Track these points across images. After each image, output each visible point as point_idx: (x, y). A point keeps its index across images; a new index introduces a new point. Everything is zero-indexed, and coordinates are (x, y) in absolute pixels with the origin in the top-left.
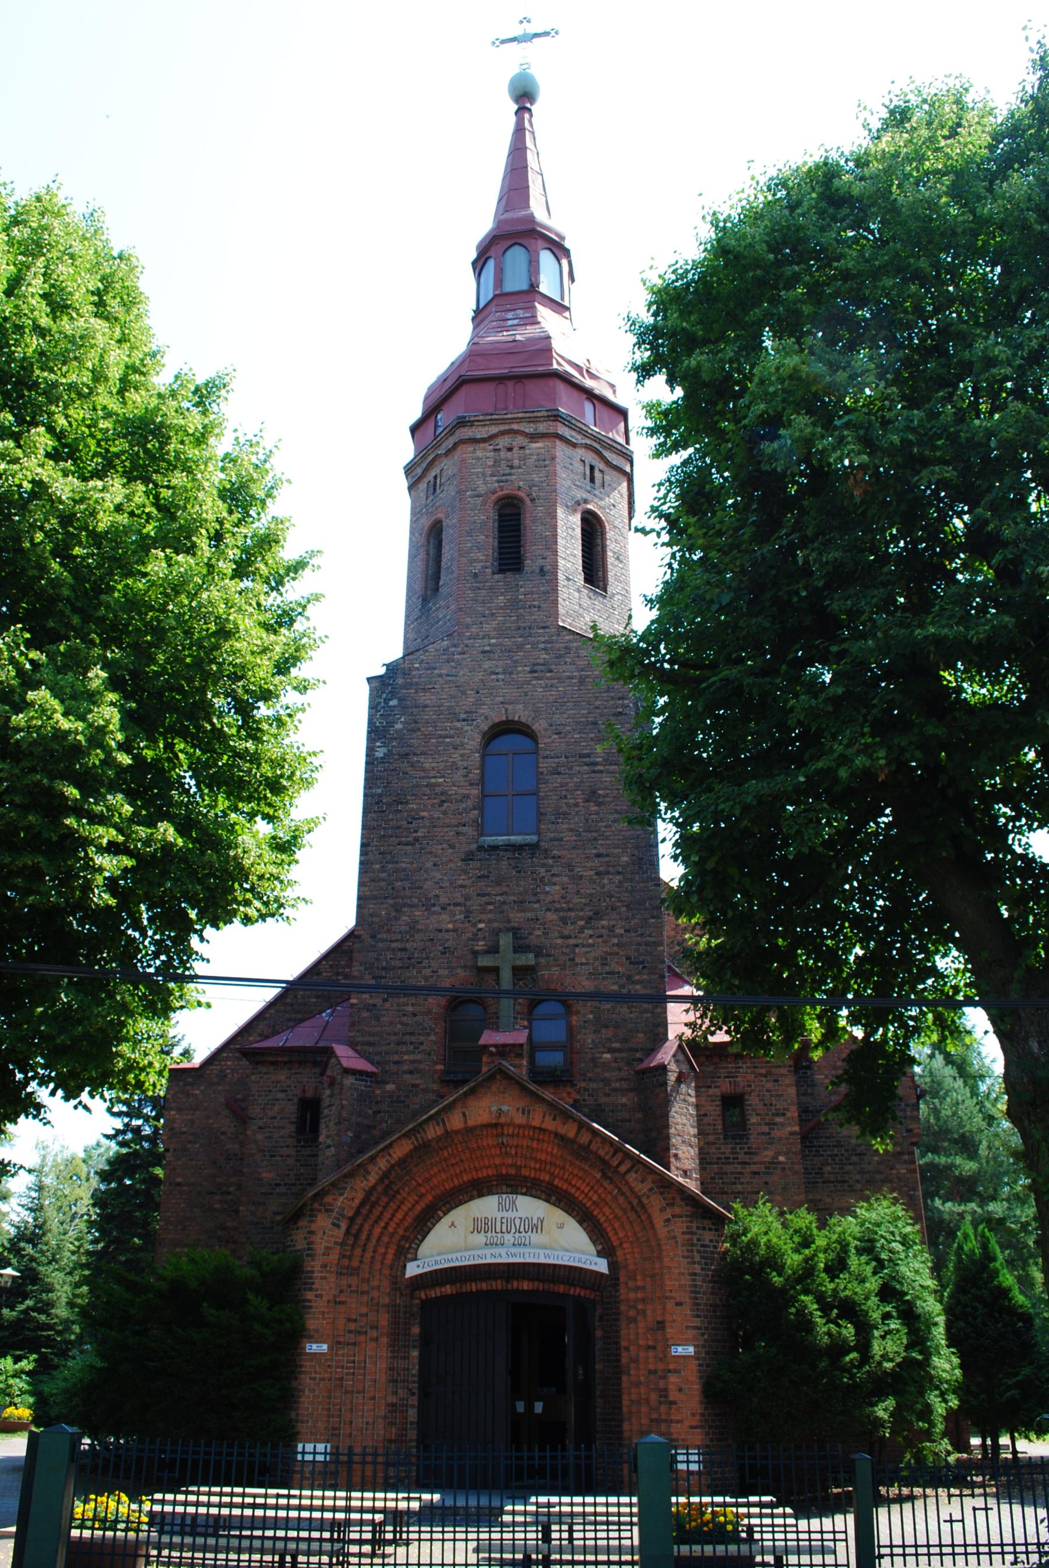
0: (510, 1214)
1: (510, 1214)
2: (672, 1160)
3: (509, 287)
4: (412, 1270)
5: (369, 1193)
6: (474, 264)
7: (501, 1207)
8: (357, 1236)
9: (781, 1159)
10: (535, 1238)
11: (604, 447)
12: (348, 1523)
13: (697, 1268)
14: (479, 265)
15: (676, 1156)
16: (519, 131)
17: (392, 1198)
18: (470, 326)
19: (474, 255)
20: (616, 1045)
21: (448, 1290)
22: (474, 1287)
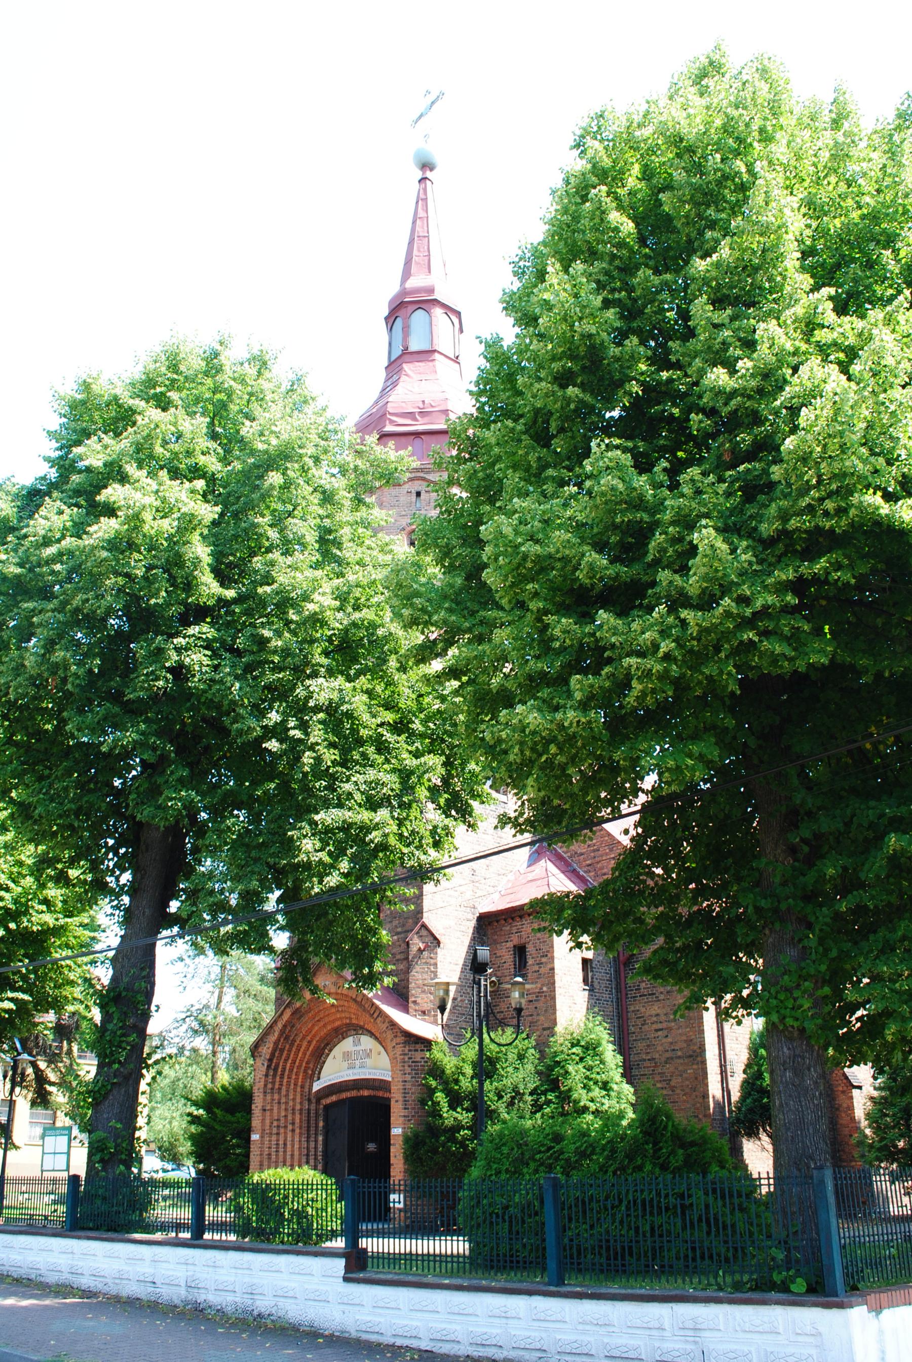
0: (358, 1048)
1: (358, 1048)
2: (411, 1005)
3: (413, 347)
4: (317, 1087)
5: (276, 1043)
6: (386, 319)
7: (355, 1044)
8: (276, 1070)
9: (545, 989)
10: (368, 1061)
11: (428, 473)
12: (442, 1192)
13: (408, 1077)
14: (391, 318)
15: (415, 1002)
16: (422, 200)
17: (292, 1045)
18: (383, 374)
19: (386, 313)
20: (399, 930)
21: (334, 1098)
22: (344, 1095)
